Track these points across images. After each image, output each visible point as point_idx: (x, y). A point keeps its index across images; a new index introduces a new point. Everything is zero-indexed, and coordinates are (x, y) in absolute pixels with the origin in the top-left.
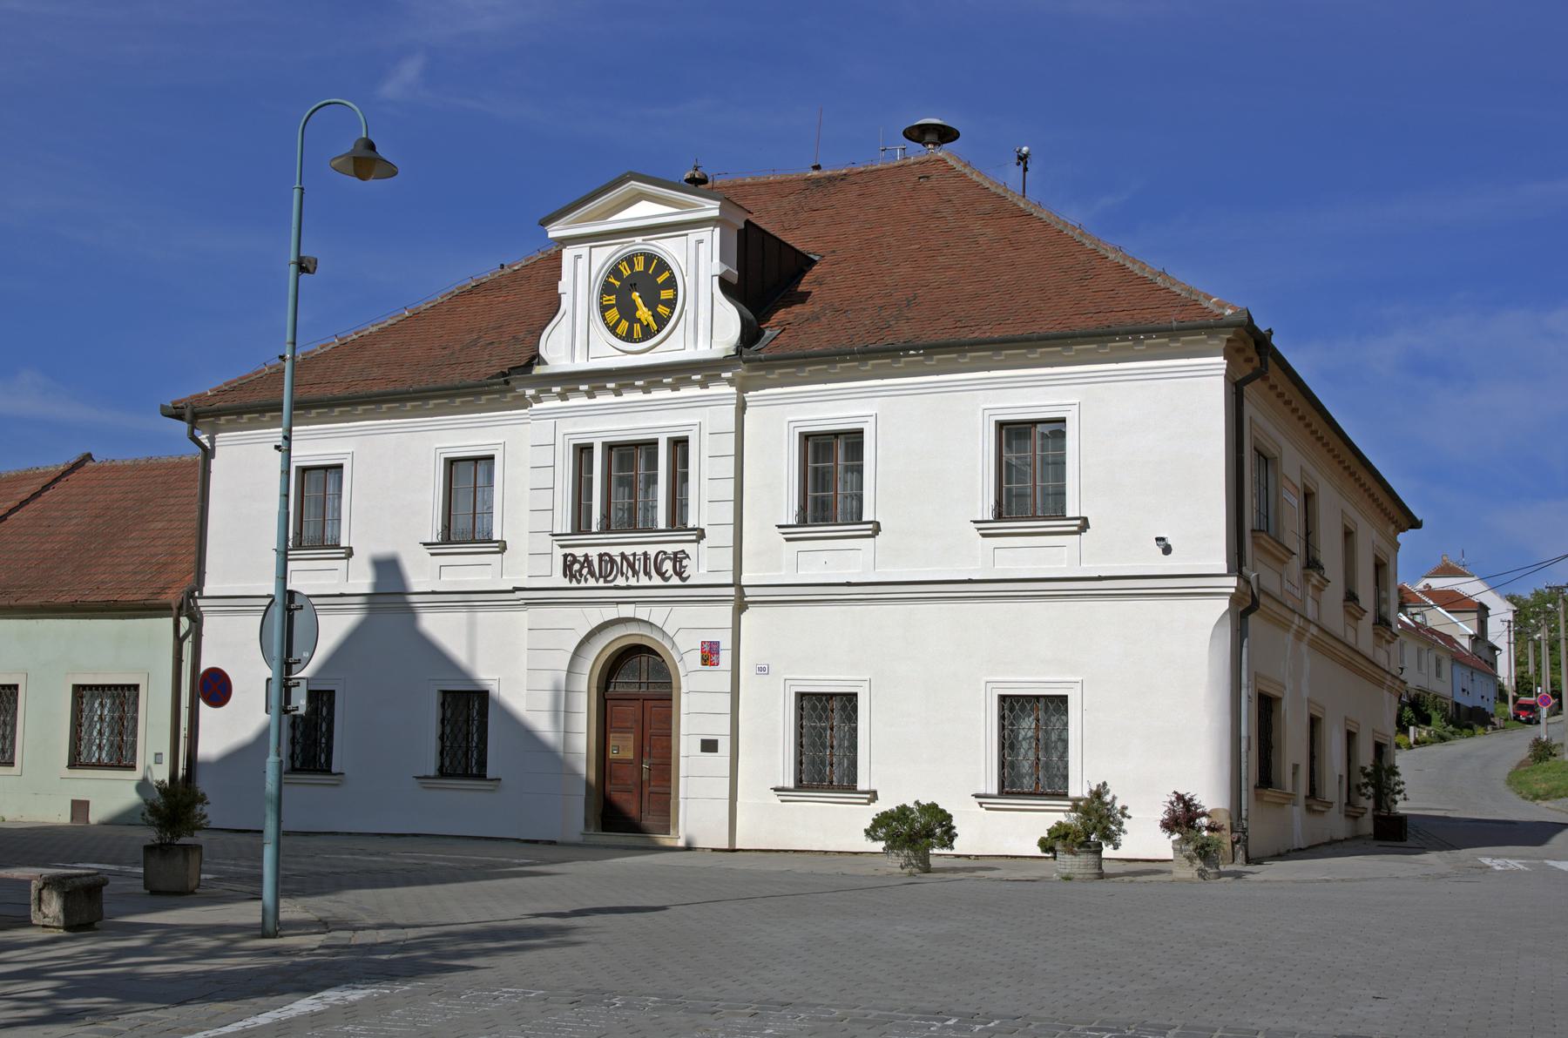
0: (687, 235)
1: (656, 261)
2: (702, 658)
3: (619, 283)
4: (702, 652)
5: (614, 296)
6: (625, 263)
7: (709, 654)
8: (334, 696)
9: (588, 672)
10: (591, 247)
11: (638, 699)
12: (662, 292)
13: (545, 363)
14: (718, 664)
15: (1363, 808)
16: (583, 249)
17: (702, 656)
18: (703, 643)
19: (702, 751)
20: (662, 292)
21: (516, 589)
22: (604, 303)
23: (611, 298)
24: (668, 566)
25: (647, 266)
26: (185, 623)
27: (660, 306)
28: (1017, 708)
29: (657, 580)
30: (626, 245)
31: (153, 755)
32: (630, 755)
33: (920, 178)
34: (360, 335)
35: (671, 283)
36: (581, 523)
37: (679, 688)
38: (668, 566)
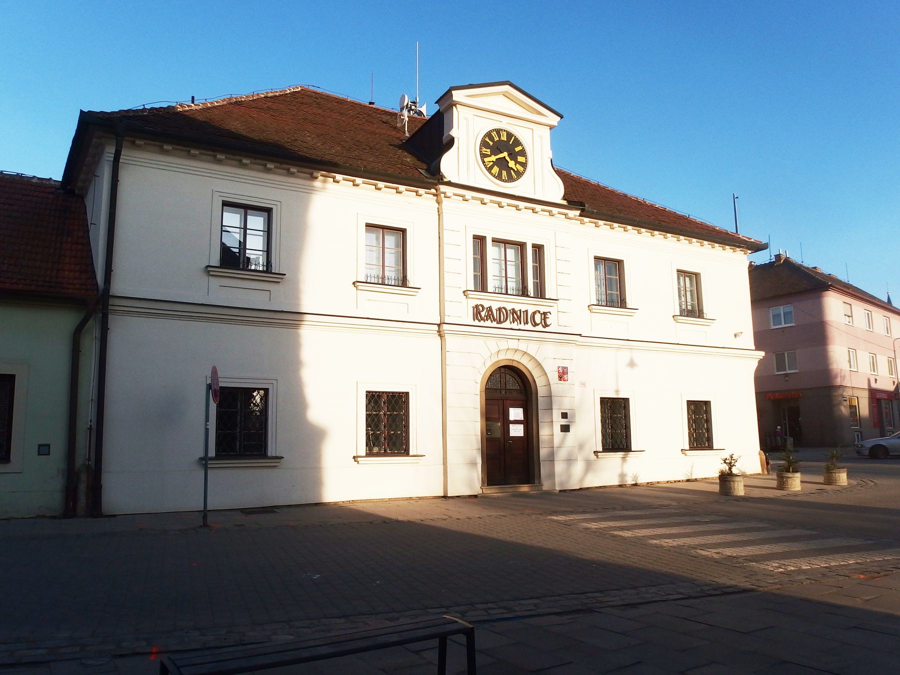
3: (492, 143)
5: (489, 150)
6: (495, 132)
18: (559, 367)
24: (538, 318)
29: (529, 326)
31: (51, 454)
36: (481, 284)
38: (538, 318)
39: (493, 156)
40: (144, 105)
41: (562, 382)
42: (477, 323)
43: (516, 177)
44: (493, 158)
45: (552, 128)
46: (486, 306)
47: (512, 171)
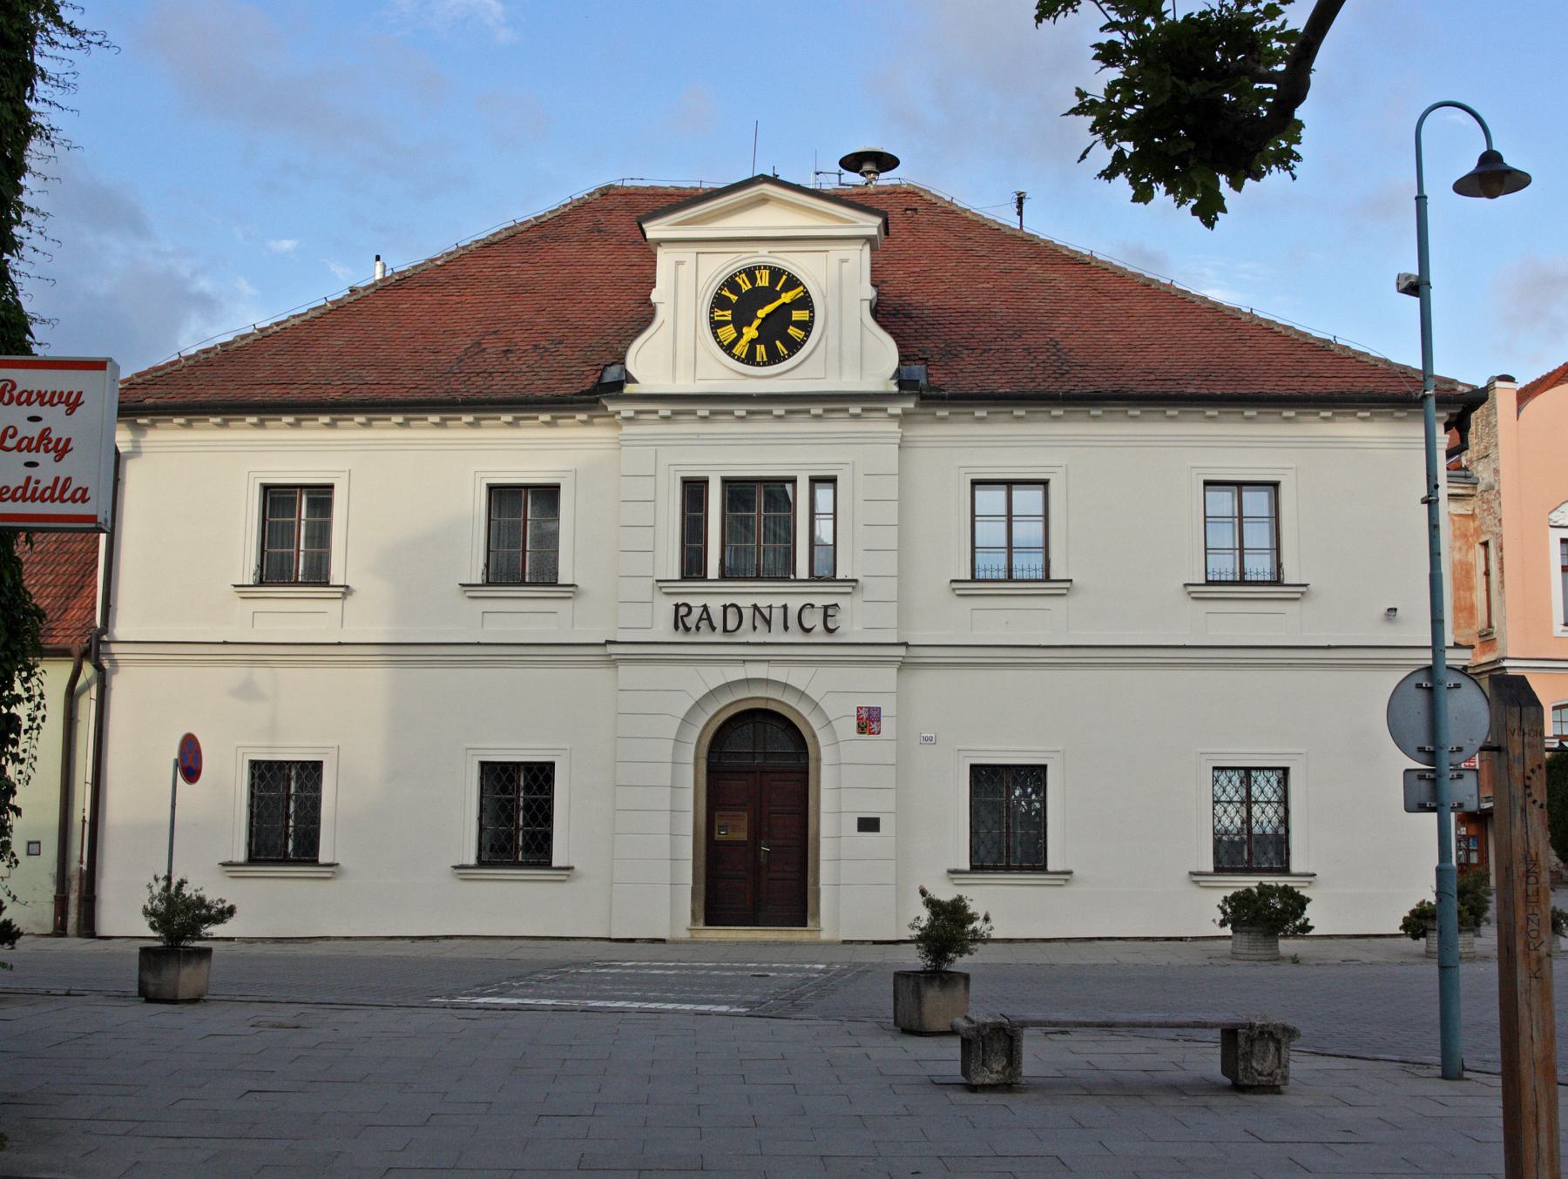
0: (828, 251)
2: (859, 726)
3: (736, 298)
4: (858, 719)
5: (730, 312)
6: (743, 275)
7: (868, 722)
8: (322, 766)
9: (695, 741)
10: (698, 253)
11: (754, 772)
12: (793, 312)
13: (634, 381)
14: (879, 733)
16: (687, 254)
17: (858, 724)
18: (859, 709)
19: (859, 831)
20: (793, 312)
21: (608, 642)
22: (716, 318)
26: (88, 670)
27: (791, 327)
28: (541, 778)
29: (796, 636)
30: (744, 255)
32: (743, 836)
33: (907, 209)
34: (282, 327)
36: (693, 567)
37: (818, 760)
38: (813, 619)
39: (745, 330)
40: (179, 353)
41: (865, 736)
42: (680, 637)
43: (786, 352)
44: (750, 332)
45: (869, 239)
46: (38, 502)
47: (29, 88)
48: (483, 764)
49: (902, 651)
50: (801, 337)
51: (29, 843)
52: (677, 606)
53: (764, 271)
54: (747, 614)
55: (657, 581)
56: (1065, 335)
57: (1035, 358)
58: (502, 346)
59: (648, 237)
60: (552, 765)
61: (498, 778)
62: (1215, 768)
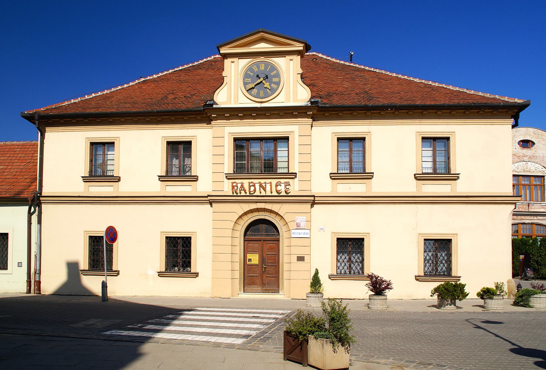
1: (270, 66)
3: (252, 74)
5: (250, 79)
6: (255, 66)
11: (261, 241)
15: (116, 271)
22: (246, 81)
23: (249, 79)
25: (266, 68)
28: (187, 242)
35: (278, 75)
48: (167, 238)
49: (312, 198)
50: (276, 88)
51: (18, 263)
52: (233, 183)
53: (262, 65)
54: (257, 186)
55: (226, 174)
56: (370, 90)
57: (360, 96)
58: (173, 97)
59: (220, 52)
60: (190, 238)
61: (172, 242)
62: (425, 240)
